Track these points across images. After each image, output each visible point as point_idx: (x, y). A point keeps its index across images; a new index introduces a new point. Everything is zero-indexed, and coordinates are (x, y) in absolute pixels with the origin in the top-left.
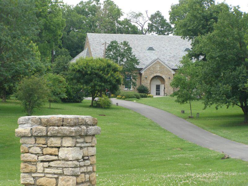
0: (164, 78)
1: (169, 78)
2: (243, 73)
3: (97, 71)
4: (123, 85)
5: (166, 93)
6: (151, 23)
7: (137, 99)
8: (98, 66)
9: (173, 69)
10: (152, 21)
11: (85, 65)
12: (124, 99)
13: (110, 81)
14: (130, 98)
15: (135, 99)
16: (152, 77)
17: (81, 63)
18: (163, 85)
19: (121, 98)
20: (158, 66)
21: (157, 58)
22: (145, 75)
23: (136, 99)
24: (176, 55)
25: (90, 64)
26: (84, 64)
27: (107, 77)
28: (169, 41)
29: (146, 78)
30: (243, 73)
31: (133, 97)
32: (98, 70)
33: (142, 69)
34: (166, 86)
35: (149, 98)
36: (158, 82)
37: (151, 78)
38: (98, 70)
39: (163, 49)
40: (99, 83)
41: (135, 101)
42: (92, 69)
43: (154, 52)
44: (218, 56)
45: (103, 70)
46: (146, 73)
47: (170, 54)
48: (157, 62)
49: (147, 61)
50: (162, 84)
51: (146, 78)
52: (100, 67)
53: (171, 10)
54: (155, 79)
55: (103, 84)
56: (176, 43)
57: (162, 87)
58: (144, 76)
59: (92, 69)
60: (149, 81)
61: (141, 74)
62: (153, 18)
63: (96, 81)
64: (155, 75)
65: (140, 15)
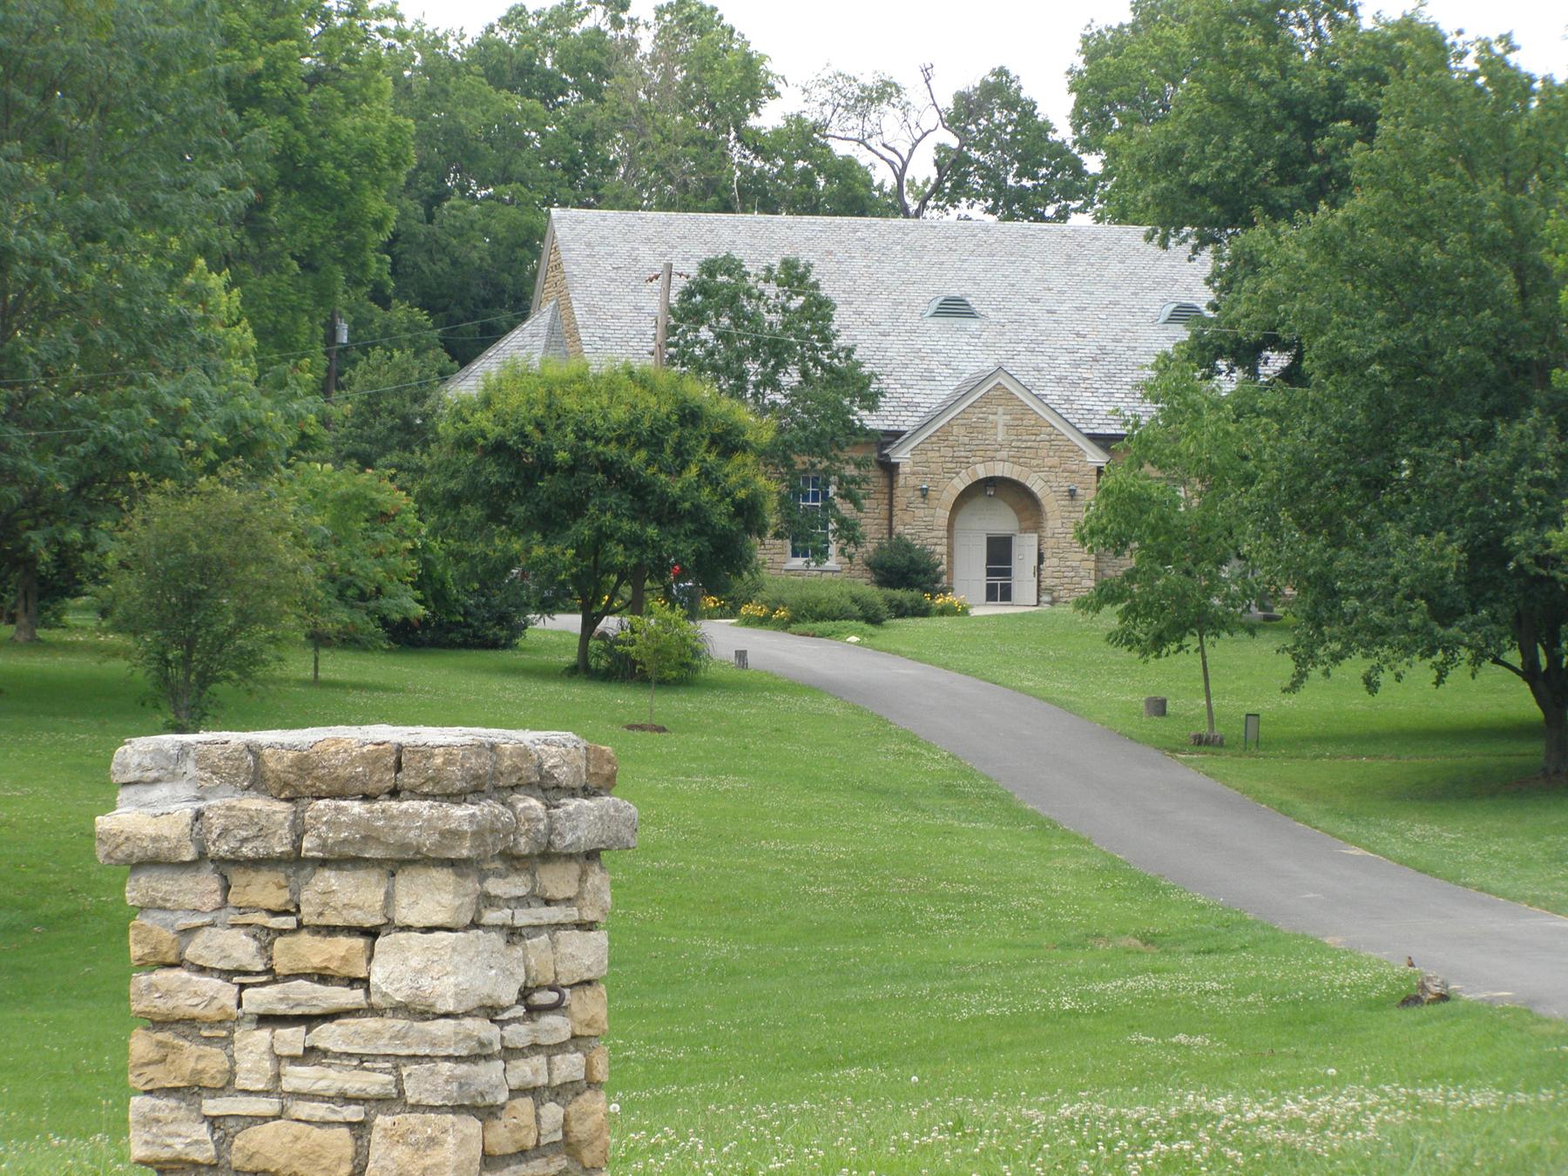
0: (1039, 495)
1: (1072, 494)
2: (1537, 464)
3: (612, 451)
4: (777, 535)
5: (1050, 590)
6: (953, 142)
7: (869, 628)
8: (619, 414)
9: (1093, 438)
10: (961, 133)
11: (539, 411)
12: (784, 625)
13: (697, 513)
14: (821, 617)
15: (853, 623)
16: (960, 484)
17: (515, 400)
18: (1033, 539)
19: (763, 622)
20: (1001, 419)
21: (990, 364)
22: (914, 474)
23: (862, 624)
24: (1110, 346)
25: (569, 402)
26: (531, 403)
27: (675, 488)
28: (1070, 260)
29: (924, 493)
30: (1537, 464)
31: (844, 615)
32: (621, 440)
33: (897, 434)
34: (1049, 542)
35: (945, 621)
36: (1002, 520)
37: (956, 493)
38: (621, 440)
39: (1034, 308)
40: (626, 525)
41: (853, 639)
42: (582, 435)
43: (973, 325)
44: (1382, 356)
45: (654, 442)
46: (924, 458)
47: (1073, 342)
48: (991, 392)
49: (928, 386)
50: (1024, 530)
51: (924, 493)
52: (636, 421)
53: (1079, 63)
54: (979, 502)
55: (652, 531)
56: (1114, 269)
57: (1024, 552)
58: (913, 481)
59: (582, 435)
60: (943, 514)
61: (890, 469)
62: (965, 110)
63: (608, 512)
64: (982, 472)
65: (885, 92)
